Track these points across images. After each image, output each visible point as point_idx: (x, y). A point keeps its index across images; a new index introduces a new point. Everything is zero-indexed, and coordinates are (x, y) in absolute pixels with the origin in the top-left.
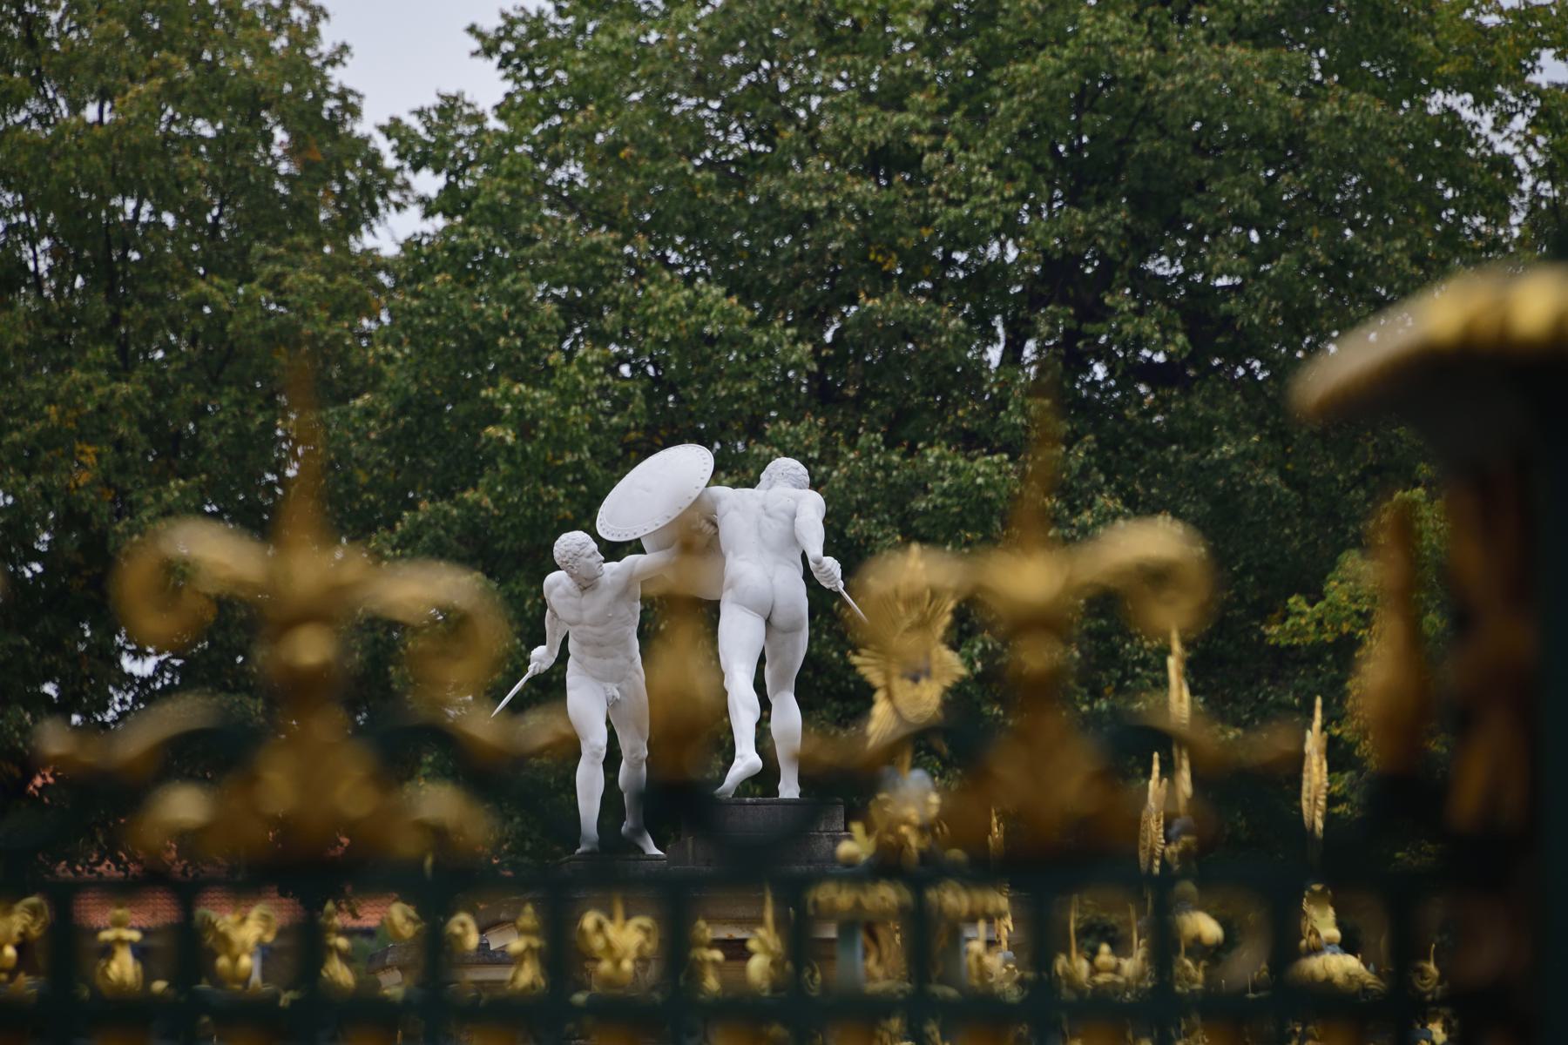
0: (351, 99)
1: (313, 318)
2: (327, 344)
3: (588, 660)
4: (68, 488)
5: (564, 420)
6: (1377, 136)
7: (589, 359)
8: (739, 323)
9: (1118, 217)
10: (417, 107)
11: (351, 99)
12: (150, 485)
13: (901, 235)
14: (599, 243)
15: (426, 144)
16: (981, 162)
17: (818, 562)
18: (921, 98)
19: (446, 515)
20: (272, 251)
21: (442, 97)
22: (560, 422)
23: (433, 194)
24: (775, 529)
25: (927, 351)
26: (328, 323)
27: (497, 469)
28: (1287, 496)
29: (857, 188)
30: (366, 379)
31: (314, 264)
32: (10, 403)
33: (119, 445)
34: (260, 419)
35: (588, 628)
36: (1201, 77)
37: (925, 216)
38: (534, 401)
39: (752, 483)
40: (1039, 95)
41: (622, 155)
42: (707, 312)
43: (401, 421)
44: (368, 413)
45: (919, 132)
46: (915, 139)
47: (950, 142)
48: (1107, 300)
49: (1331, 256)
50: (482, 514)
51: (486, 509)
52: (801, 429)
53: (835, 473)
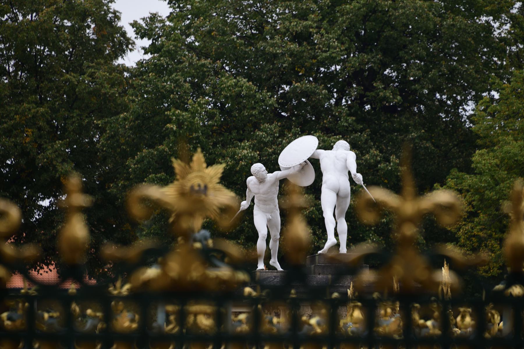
0: (117, 14)
1: (105, 87)
2: (110, 96)
3: (261, 206)
4: (22, 143)
5: (193, 122)
6: (465, 30)
7: (202, 102)
8: (252, 91)
9: (378, 57)
10: (143, 17)
11: (117, 14)
12: (49, 142)
13: (306, 62)
14: (204, 63)
15: (146, 29)
16: (333, 38)
17: (355, 175)
18: (313, 16)
19: (152, 153)
20: (91, 64)
21: (151, 14)
22: (192, 123)
23: (147, 46)
24: (340, 164)
25: (315, 101)
26: (110, 89)
27: (170, 139)
28: (433, 150)
29: (292, 46)
30: (122, 108)
31: (105, 69)
32: (3, 114)
33: (40, 129)
34: (87, 121)
35: (262, 195)
36: (408, 10)
37: (314, 55)
38: (183, 116)
39: (331, 150)
40: (353, 16)
41: (212, 34)
42: (242, 87)
43: (137, 122)
44: (125, 119)
45: (312, 28)
46: (311, 30)
47: (323, 31)
48: (374, 84)
49: (449, 71)
50: (165, 153)
51: (166, 152)
52: (272, 127)
53: (284, 141)
